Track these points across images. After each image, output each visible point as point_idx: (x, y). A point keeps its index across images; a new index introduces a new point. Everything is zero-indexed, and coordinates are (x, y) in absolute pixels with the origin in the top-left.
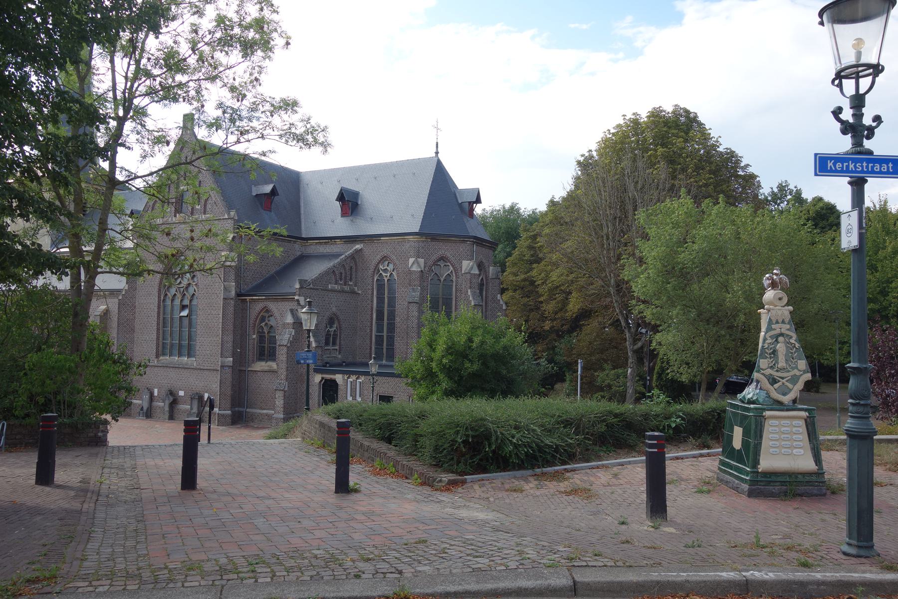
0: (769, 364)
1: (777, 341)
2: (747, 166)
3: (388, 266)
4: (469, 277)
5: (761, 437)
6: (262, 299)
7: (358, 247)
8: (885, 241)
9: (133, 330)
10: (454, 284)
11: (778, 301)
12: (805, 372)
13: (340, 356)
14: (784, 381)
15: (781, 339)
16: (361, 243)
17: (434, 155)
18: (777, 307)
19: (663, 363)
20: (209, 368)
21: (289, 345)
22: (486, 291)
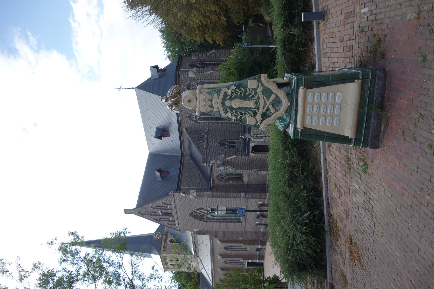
0: (252, 116)
1: (231, 108)
3: (193, 116)
4: (198, 73)
5: (321, 132)
6: (212, 179)
7: (184, 130)
9: (229, 232)
10: (202, 81)
11: (192, 103)
12: (259, 81)
13: (240, 140)
14: (268, 103)
15: (227, 103)
16: (182, 129)
17: (134, 90)
20: (246, 202)
21: (235, 169)
22: (205, 61)
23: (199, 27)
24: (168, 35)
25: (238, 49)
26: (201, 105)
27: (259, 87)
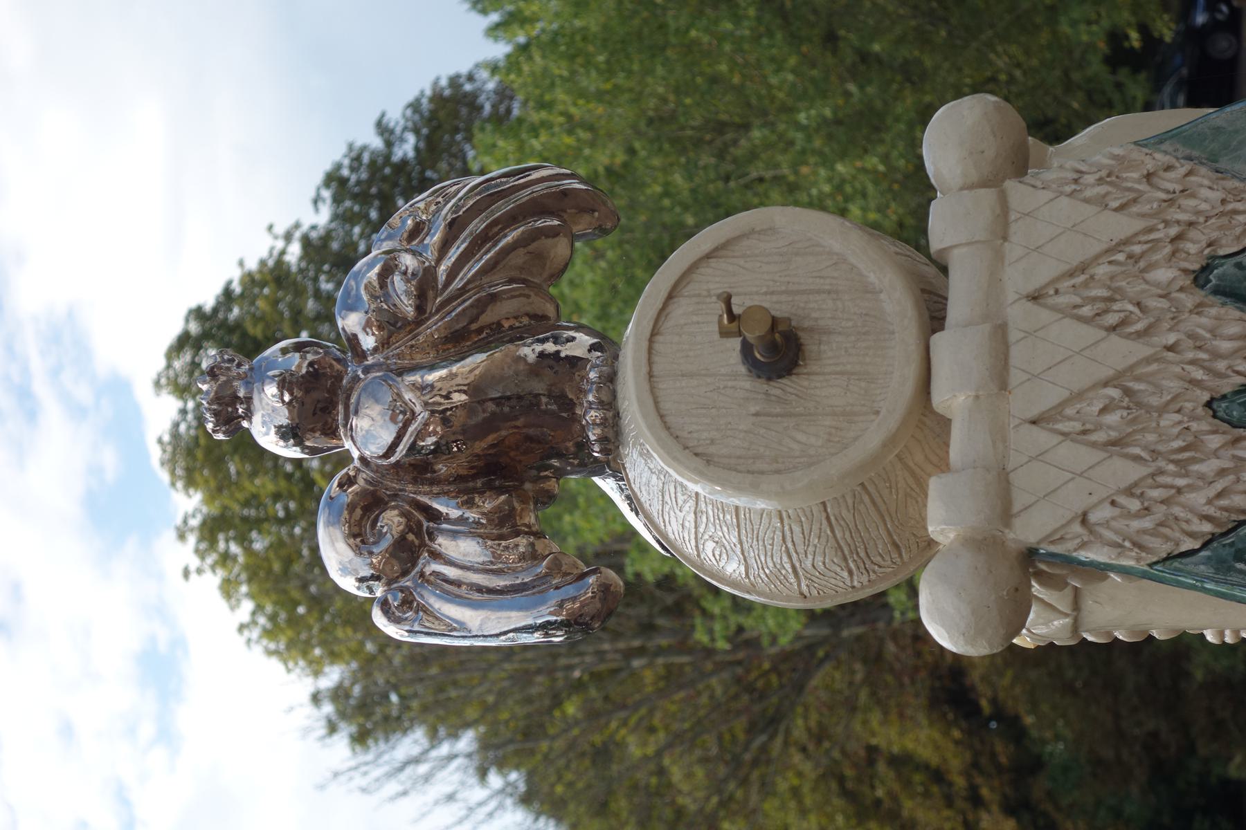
2: (382, 128)
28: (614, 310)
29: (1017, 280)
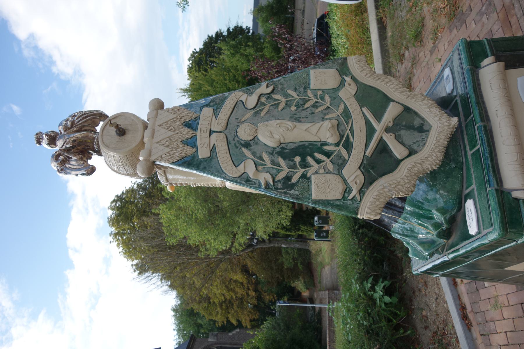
8: (204, 90)
11: (128, 137)
14: (378, 127)
18: (146, 140)
19: (278, 228)
22: (226, 344)
23: (221, 305)
24: (182, 314)
25: (270, 324)
26: (156, 139)
27: (346, 84)
28: (187, 197)
29: (158, 123)
